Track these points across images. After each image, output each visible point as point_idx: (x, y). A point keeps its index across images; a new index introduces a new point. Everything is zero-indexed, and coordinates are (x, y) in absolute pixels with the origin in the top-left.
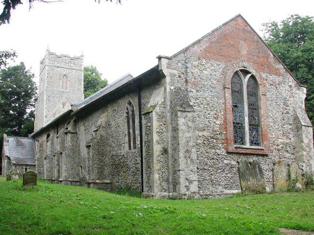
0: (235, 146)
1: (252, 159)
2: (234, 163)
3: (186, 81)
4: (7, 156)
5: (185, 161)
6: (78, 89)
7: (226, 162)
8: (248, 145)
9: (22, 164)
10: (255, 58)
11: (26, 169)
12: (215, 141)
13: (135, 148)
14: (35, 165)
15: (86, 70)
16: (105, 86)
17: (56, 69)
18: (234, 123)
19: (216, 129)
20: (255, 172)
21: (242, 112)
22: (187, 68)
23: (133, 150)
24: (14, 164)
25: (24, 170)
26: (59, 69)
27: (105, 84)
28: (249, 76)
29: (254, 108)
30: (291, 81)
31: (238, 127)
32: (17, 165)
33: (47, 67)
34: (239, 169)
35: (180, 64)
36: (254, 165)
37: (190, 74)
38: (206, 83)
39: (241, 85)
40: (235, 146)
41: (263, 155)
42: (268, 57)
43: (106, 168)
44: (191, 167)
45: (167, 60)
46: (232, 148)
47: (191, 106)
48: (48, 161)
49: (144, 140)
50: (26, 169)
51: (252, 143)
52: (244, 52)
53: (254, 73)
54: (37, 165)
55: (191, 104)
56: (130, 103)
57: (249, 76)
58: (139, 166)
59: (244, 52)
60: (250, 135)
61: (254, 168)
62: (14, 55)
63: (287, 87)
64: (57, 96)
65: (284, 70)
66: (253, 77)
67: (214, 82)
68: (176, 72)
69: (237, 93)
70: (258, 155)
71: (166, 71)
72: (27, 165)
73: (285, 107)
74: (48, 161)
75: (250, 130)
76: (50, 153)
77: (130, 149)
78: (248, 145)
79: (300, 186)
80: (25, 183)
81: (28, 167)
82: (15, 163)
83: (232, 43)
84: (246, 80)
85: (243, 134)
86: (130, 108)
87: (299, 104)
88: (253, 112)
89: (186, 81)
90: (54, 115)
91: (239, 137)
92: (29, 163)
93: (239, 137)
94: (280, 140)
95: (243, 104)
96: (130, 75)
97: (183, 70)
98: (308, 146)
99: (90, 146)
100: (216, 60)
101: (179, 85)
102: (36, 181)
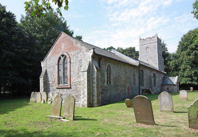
26: (145, 45)
73: (80, 64)
98: (84, 81)
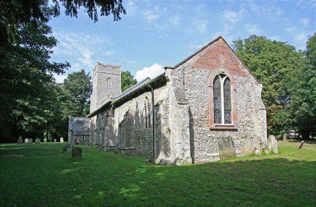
0: (215, 125)
1: (227, 134)
2: (214, 135)
3: (184, 83)
5: (182, 137)
6: (118, 87)
7: (209, 135)
8: (223, 124)
10: (230, 66)
11: (83, 138)
12: (202, 122)
13: (150, 127)
15: (123, 74)
16: (135, 84)
17: (103, 74)
18: (214, 109)
19: (202, 114)
20: (229, 144)
21: (220, 102)
22: (184, 74)
23: (148, 129)
24: (76, 135)
27: (136, 82)
28: (225, 77)
29: (227, 98)
30: (253, 80)
31: (217, 111)
34: (219, 142)
35: (179, 72)
36: (229, 138)
37: (186, 78)
38: (197, 84)
39: (220, 84)
40: (215, 125)
41: (233, 130)
42: (238, 65)
43: (131, 139)
44: (186, 141)
45: (171, 70)
46: (213, 126)
47: (186, 100)
49: (155, 123)
50: (83, 138)
51: (226, 122)
52: (222, 62)
53: (228, 75)
55: (187, 98)
56: (147, 98)
57: (225, 77)
58: (152, 139)
59: (222, 62)
60: (225, 117)
61: (228, 141)
62: (68, 65)
63: (250, 84)
65: (249, 73)
66: (228, 79)
67: (202, 83)
68: (176, 77)
69: (216, 90)
70: (229, 130)
71: (170, 77)
72: (84, 135)
75: (225, 113)
77: (147, 128)
78: (223, 124)
80: (74, 155)
83: (215, 56)
84: (214, 63)
85: (221, 116)
86: (147, 101)
87: (258, 95)
88: (227, 102)
89: (184, 83)
90: (102, 103)
91: (217, 119)
92: (85, 134)
93: (217, 119)
94: (244, 119)
95: (220, 97)
96: (148, 78)
97: (182, 76)
99: (121, 126)
100: (204, 68)
101: (179, 86)
102: (81, 153)
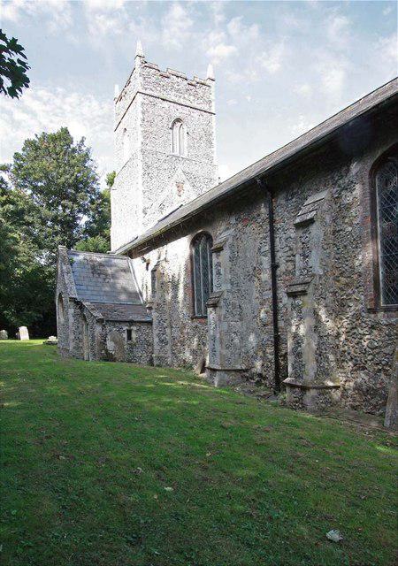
4: (73, 300)
9: (119, 319)
11: (129, 332)
14: (150, 323)
24: (100, 321)
25: (125, 335)
26: (166, 104)
32: (107, 321)
33: (140, 98)
48: (223, 312)
50: (129, 332)
54: (155, 322)
64: (165, 166)
72: (132, 322)
74: (223, 312)
76: (229, 286)
79: (251, 337)
81: (134, 328)
82: (100, 316)
90: (162, 206)
